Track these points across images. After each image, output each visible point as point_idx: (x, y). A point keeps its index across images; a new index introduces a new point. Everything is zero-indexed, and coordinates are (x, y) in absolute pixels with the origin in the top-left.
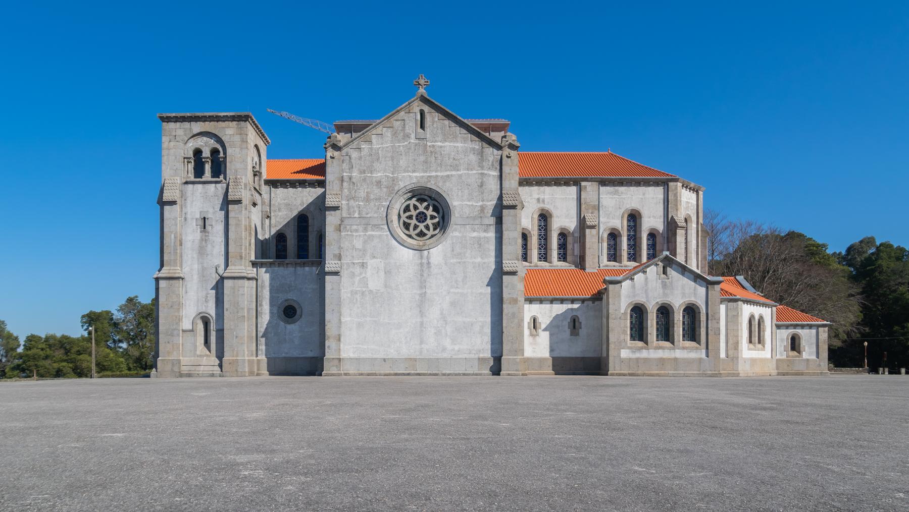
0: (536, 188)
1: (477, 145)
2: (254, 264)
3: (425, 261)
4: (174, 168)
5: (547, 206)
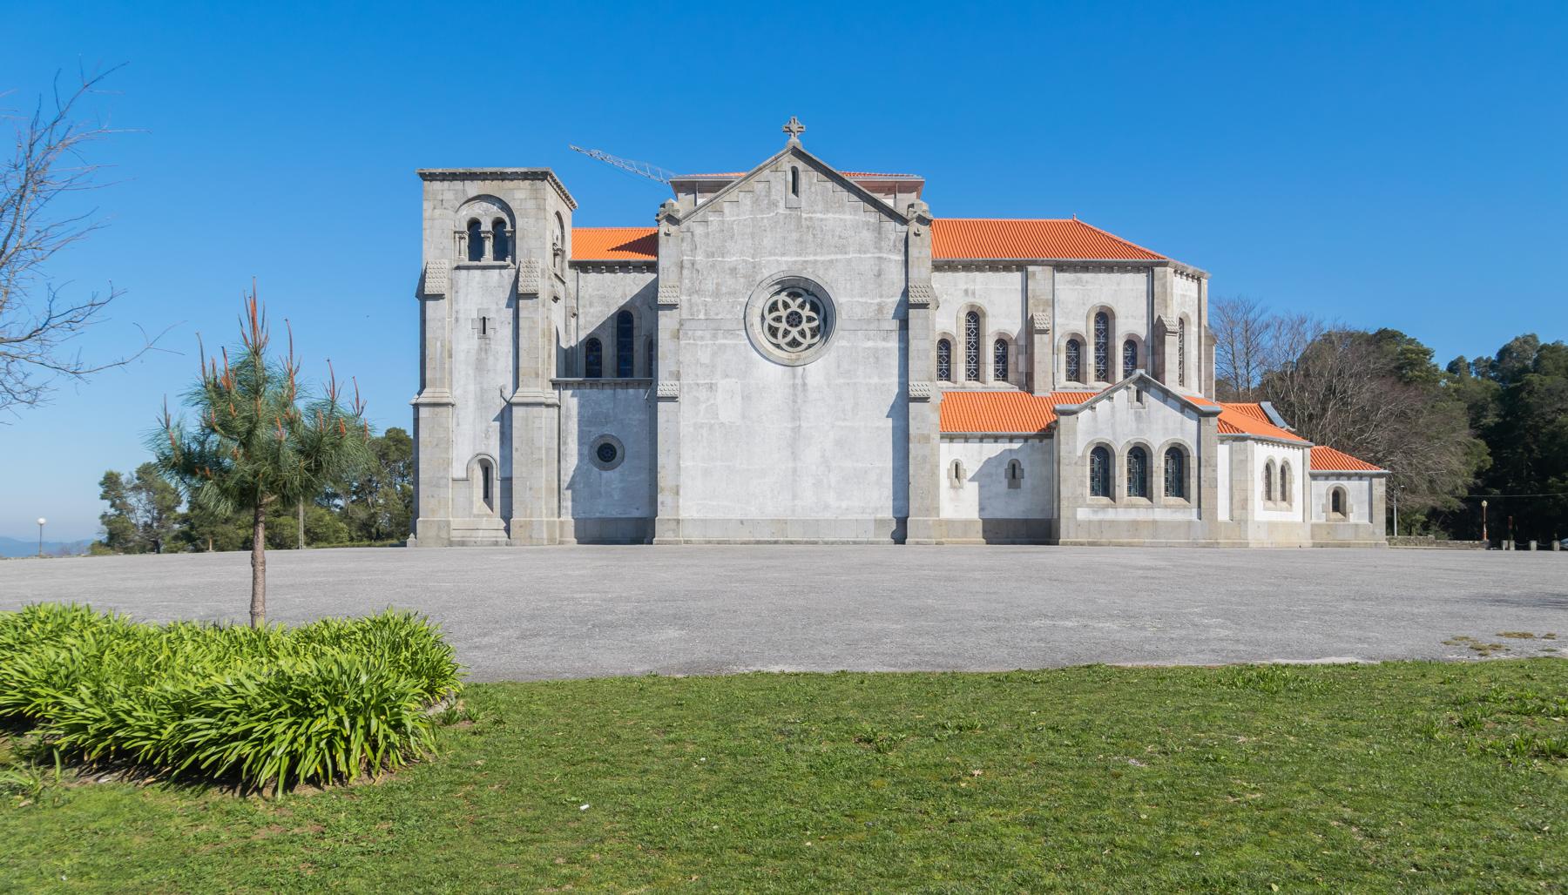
0: (963, 274)
1: (873, 216)
2: (555, 385)
3: (799, 381)
4: (440, 248)
5: (979, 301)
